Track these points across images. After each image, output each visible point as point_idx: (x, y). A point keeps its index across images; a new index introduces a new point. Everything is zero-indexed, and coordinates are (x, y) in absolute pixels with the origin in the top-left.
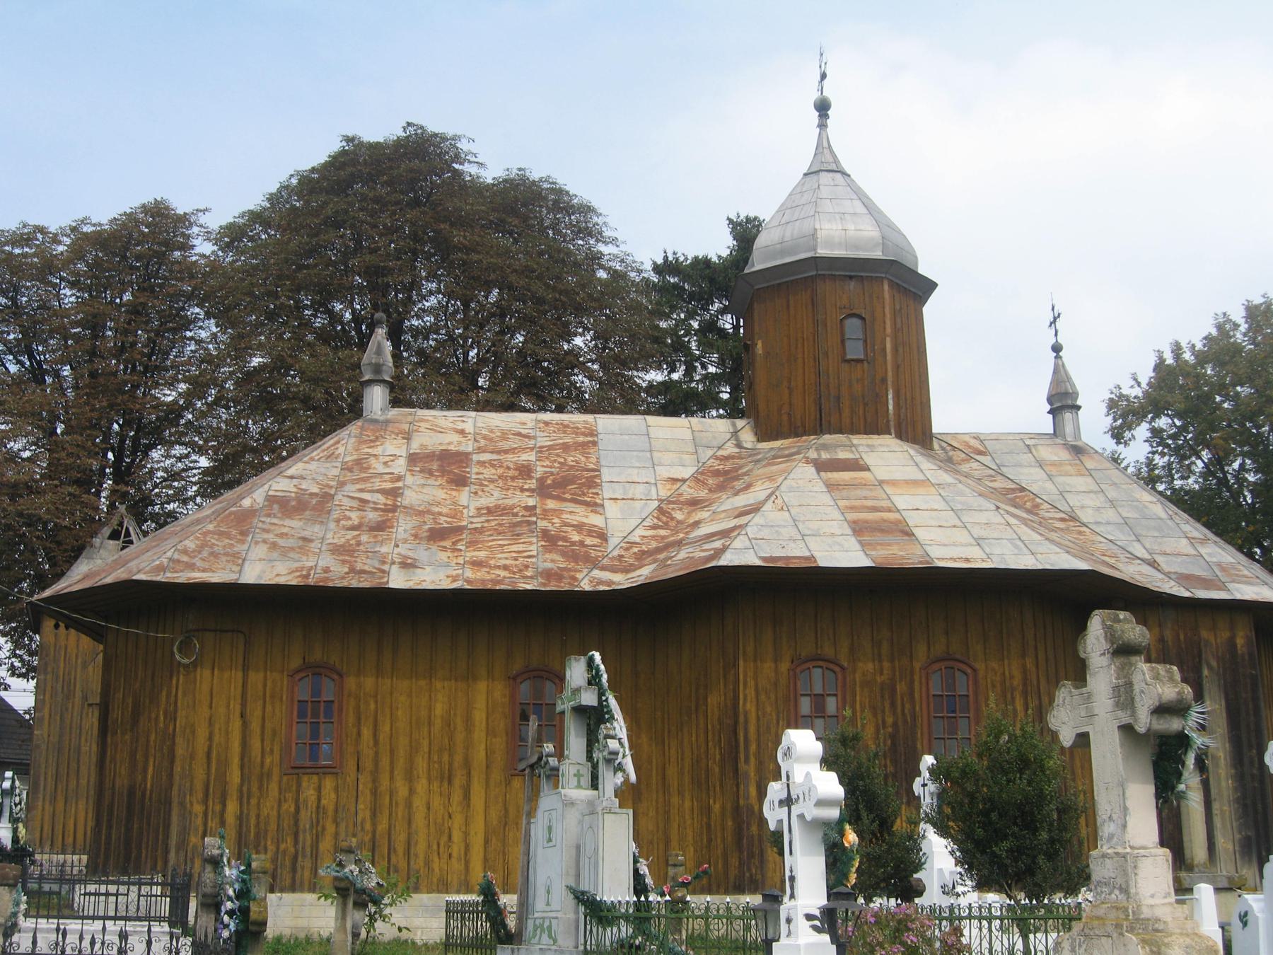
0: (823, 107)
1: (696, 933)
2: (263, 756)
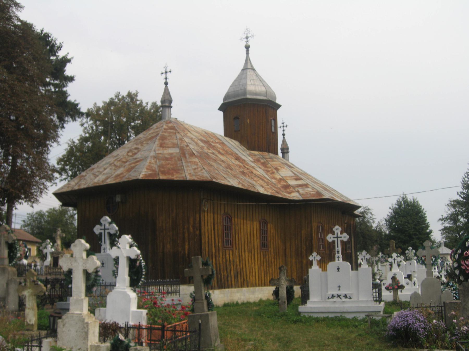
0: (247, 47)
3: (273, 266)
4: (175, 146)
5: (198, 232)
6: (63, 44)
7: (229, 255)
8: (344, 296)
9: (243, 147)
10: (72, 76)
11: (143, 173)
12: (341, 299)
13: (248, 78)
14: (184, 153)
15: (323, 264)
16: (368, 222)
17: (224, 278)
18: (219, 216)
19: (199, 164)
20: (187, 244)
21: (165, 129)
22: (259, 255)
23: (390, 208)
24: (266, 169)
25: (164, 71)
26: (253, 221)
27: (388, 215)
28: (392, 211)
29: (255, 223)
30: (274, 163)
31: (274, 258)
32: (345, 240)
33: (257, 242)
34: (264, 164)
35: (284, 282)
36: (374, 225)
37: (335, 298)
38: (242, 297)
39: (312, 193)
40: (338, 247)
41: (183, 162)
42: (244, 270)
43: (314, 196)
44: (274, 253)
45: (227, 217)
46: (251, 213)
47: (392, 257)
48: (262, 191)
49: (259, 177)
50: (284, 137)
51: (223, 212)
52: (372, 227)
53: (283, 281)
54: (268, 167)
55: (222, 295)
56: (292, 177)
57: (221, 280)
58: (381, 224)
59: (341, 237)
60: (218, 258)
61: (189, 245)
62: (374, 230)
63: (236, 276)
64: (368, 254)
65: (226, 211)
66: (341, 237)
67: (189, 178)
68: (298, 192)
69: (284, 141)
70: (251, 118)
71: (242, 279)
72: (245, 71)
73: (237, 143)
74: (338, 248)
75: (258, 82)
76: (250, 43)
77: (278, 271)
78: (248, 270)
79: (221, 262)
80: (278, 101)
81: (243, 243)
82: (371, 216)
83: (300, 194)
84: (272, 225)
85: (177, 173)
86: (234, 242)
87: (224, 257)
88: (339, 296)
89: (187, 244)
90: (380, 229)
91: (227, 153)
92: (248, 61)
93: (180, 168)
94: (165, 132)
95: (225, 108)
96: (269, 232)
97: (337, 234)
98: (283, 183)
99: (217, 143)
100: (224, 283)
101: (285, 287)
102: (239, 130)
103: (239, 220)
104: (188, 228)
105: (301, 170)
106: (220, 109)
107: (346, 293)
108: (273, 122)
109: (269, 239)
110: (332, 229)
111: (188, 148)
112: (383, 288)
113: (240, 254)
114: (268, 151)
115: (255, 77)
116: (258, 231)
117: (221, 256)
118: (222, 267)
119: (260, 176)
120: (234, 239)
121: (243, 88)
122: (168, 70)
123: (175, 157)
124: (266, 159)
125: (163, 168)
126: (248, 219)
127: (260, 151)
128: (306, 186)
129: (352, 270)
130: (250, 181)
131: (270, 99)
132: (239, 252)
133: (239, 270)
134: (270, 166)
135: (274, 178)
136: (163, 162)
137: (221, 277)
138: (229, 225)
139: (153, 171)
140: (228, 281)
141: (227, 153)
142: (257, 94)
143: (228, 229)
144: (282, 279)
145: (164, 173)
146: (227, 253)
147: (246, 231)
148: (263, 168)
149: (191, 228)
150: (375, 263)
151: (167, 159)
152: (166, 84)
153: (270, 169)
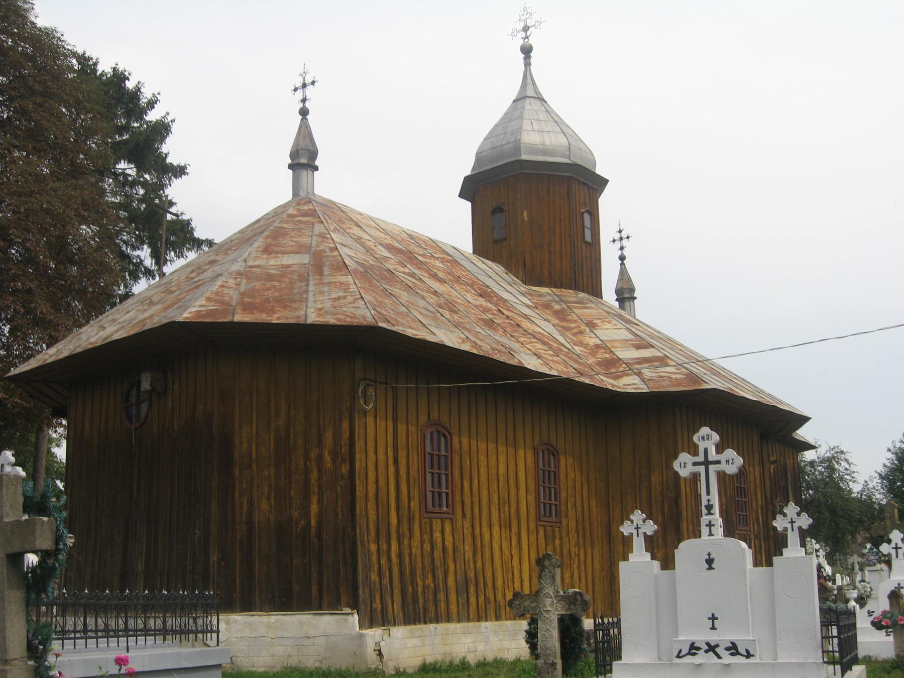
0: (527, 51)
1: (178, 636)
2: (409, 502)
3: (575, 566)
4: (301, 249)
5: (345, 469)
6: (158, 96)
7: (443, 532)
8: (727, 649)
9: (510, 278)
10: (183, 164)
11: (194, 310)
12: (719, 657)
13: (527, 115)
14: (323, 263)
15: (663, 549)
16: (841, 478)
17: (424, 593)
18: (412, 429)
19: (353, 288)
20: (314, 500)
21: (289, 216)
22: (533, 537)
23: (889, 450)
24: (565, 324)
25: (299, 84)
26: (515, 446)
27: (885, 466)
28: (894, 457)
29: (521, 452)
30: (587, 311)
31: (578, 544)
32: (732, 470)
33: (526, 501)
34: (561, 315)
35: (552, 604)
36: (856, 488)
37: (701, 652)
38: (481, 647)
39: (674, 376)
40: (708, 493)
41: (311, 283)
42: (489, 574)
43: (679, 385)
45: (438, 431)
47: (889, 541)
48: (532, 363)
49: (535, 337)
50: (622, 264)
51: (423, 419)
52: (850, 492)
53: (548, 601)
55: (416, 641)
56: (627, 341)
57: (415, 600)
58: (871, 485)
59: (718, 462)
60: (406, 541)
61: (320, 502)
62: (854, 498)
63: (463, 588)
64: (804, 515)
65: (435, 415)
66: (718, 462)
67: (313, 318)
68: (639, 374)
69: (623, 274)
70: (537, 208)
71: (481, 598)
72: (520, 103)
73: (499, 268)
75: (551, 126)
76: (532, 41)
77: (537, 569)
78: (499, 575)
79: (416, 551)
80: (599, 171)
81: (485, 502)
82: (847, 466)
83: (643, 380)
84: (570, 460)
86: (458, 498)
87: (426, 537)
88: (712, 648)
89: (314, 500)
90: (870, 498)
91: (458, 280)
92: (529, 81)
93: (297, 297)
94: (288, 222)
95: (471, 189)
96: (562, 477)
97: (706, 450)
98: (602, 355)
99: (437, 258)
100: (425, 610)
101: (554, 618)
102: (505, 239)
103: (474, 442)
104: (320, 459)
105: (659, 332)
106: (461, 195)
107: (734, 638)
108: (587, 217)
109: (564, 495)
110: (690, 439)
111: (336, 253)
112: (863, 622)
113: (477, 532)
114: (576, 287)
115: (542, 116)
116: (531, 474)
117: (417, 534)
118: (419, 565)
119: (538, 336)
120: (457, 491)
121: (512, 140)
122: (309, 80)
123: (292, 272)
124: (565, 302)
125: (252, 296)
126: (501, 439)
127: (556, 287)
128: (662, 361)
129: (756, 564)
130: (504, 340)
131: (579, 163)
132: (473, 527)
134: (575, 318)
136: (258, 285)
137: (415, 592)
138: (443, 452)
139: (223, 303)
140: (436, 603)
141: (458, 280)
142: (545, 152)
143: (440, 463)
144: (547, 595)
145: (248, 308)
146: (437, 526)
147: (493, 471)
148: (556, 321)
149: (327, 458)
150: (857, 567)
151: (270, 277)
152: (304, 112)
153: (573, 325)
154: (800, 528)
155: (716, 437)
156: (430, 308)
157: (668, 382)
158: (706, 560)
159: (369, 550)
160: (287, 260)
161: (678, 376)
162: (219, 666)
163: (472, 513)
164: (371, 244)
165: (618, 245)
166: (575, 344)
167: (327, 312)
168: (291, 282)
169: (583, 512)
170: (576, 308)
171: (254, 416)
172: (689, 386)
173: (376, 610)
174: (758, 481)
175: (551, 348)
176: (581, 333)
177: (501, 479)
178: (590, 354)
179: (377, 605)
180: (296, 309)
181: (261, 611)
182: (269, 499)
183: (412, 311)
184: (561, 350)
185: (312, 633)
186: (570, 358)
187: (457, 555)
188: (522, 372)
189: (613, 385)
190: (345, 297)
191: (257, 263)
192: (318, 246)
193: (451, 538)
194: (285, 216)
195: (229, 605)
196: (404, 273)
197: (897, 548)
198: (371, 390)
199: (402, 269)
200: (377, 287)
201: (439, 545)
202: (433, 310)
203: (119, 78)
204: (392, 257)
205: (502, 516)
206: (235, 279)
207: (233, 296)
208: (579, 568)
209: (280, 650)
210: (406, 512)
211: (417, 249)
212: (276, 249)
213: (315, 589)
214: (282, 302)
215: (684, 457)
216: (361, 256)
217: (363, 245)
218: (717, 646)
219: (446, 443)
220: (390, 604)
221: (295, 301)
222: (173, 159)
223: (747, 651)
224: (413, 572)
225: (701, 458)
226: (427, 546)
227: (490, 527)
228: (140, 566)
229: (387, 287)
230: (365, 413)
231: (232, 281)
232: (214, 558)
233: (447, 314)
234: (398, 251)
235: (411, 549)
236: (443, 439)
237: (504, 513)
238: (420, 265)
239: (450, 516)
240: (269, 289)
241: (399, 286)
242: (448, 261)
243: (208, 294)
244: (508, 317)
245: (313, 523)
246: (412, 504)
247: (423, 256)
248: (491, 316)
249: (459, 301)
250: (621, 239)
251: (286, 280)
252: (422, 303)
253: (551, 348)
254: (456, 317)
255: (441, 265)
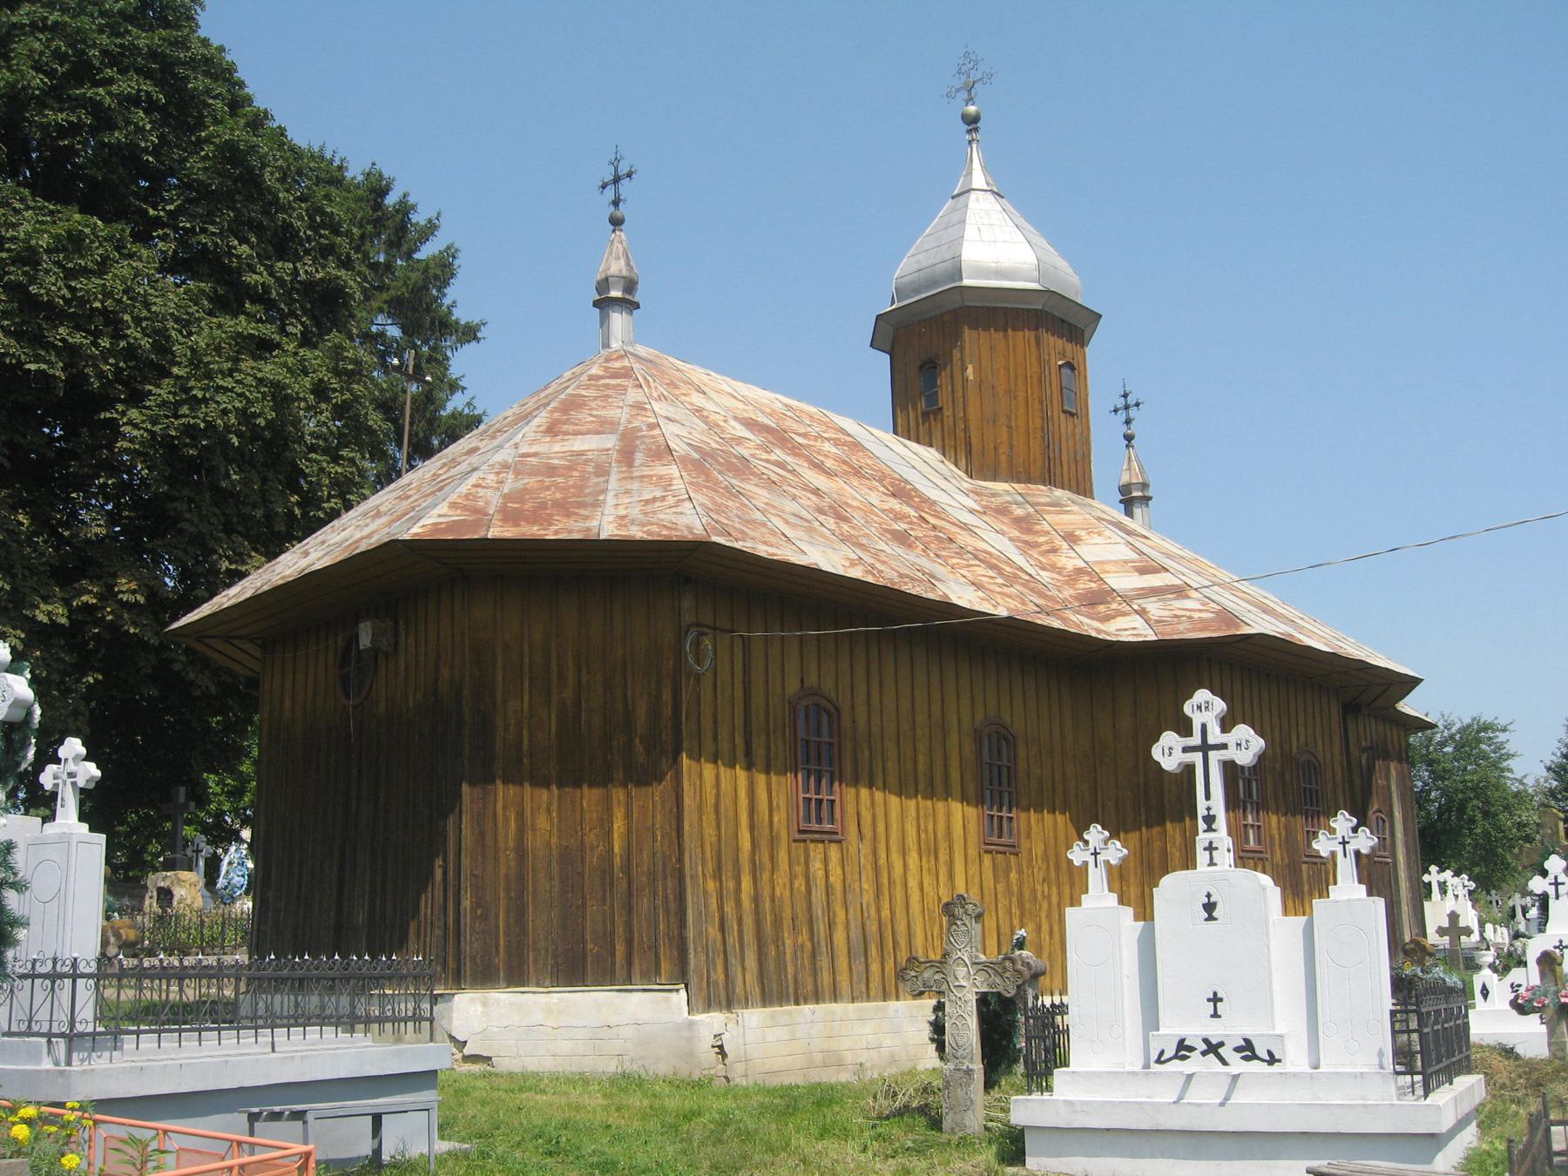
3: (1043, 914)
4: (604, 426)
7: (826, 861)
8: (1238, 1049)
12: (1224, 1063)
13: (971, 218)
19: (678, 485)
21: (591, 378)
22: (974, 869)
25: (609, 178)
37: (1195, 1055)
39: (1196, 615)
40: (1208, 797)
41: (614, 477)
42: (901, 927)
44: (1046, 859)
46: (936, 695)
48: (964, 597)
49: (976, 557)
53: (961, 971)
54: (1036, 533)
55: (782, 1033)
56: (1126, 562)
59: (1224, 746)
60: (766, 876)
61: (628, 815)
66: (1224, 746)
68: (1142, 613)
73: (931, 454)
74: (1212, 800)
85: (568, 515)
87: (799, 869)
88: (1212, 1048)
91: (857, 472)
94: (588, 387)
98: (1084, 584)
99: (828, 439)
107: (1248, 1032)
111: (656, 432)
113: (882, 861)
114: (1050, 479)
119: (982, 555)
122: (623, 170)
123: (586, 462)
125: (521, 500)
132: (875, 853)
133: (873, 928)
134: (1047, 527)
135: (1053, 568)
136: (531, 482)
138: (825, 738)
139: (476, 511)
145: (508, 516)
151: (551, 470)
153: (1042, 539)
154: (1357, 853)
155: (1219, 705)
156: (804, 514)
157: (1186, 625)
158: (1204, 906)
159: (705, 891)
160: (578, 444)
161: (1204, 615)
162: (427, 1078)
163: (874, 832)
164: (719, 419)
165: (1122, 415)
166: (1043, 569)
167: (633, 522)
168: (582, 478)
169: (1055, 830)
170: (1049, 512)
171: (526, 684)
172: (1220, 629)
173: (716, 983)
174: (1339, 779)
175: (1000, 572)
176: (1054, 551)
177: (921, 778)
178: (1067, 583)
179: (719, 976)
180: (586, 518)
181: (538, 985)
182: (549, 810)
183: (773, 519)
184: (1016, 577)
185: (613, 1021)
186: (1032, 590)
187: (849, 897)
188: (949, 609)
189: (1099, 631)
190: (663, 498)
191: (534, 449)
192: (630, 422)
193: (839, 871)
194: (584, 378)
195: (458, 980)
196: (767, 461)
197: (1556, 884)
198: (707, 642)
199: (765, 456)
200: (717, 482)
201: (821, 882)
202: (809, 517)
203: (377, 188)
204: (752, 437)
205: (923, 836)
206: (498, 473)
207: (492, 500)
208: (1049, 916)
209: (564, 1046)
210: (766, 831)
211: (795, 426)
212: (565, 428)
213: (620, 949)
214: (564, 508)
215: (1169, 738)
216: (699, 434)
217: (705, 419)
218: (1222, 1044)
219: (830, 723)
220: (739, 975)
221: (583, 505)
222: (462, 315)
223: (1270, 1053)
224: (777, 923)
225: (1196, 740)
226: (800, 884)
227: (904, 853)
228: (361, 917)
229: (734, 481)
230: (698, 677)
231: (492, 477)
232: (466, 903)
233: (831, 522)
234: (765, 429)
235: (773, 888)
236: (825, 719)
237: (926, 831)
238: (795, 450)
239: (839, 837)
240: (548, 488)
241: (755, 480)
242: (845, 444)
243: (453, 497)
244: (935, 527)
245: (616, 849)
246: (776, 819)
247: (804, 435)
248: (905, 526)
249: (855, 503)
250: (1127, 407)
251: (575, 474)
252: (790, 506)
253: (1000, 572)
254: (845, 527)
255: (834, 450)
